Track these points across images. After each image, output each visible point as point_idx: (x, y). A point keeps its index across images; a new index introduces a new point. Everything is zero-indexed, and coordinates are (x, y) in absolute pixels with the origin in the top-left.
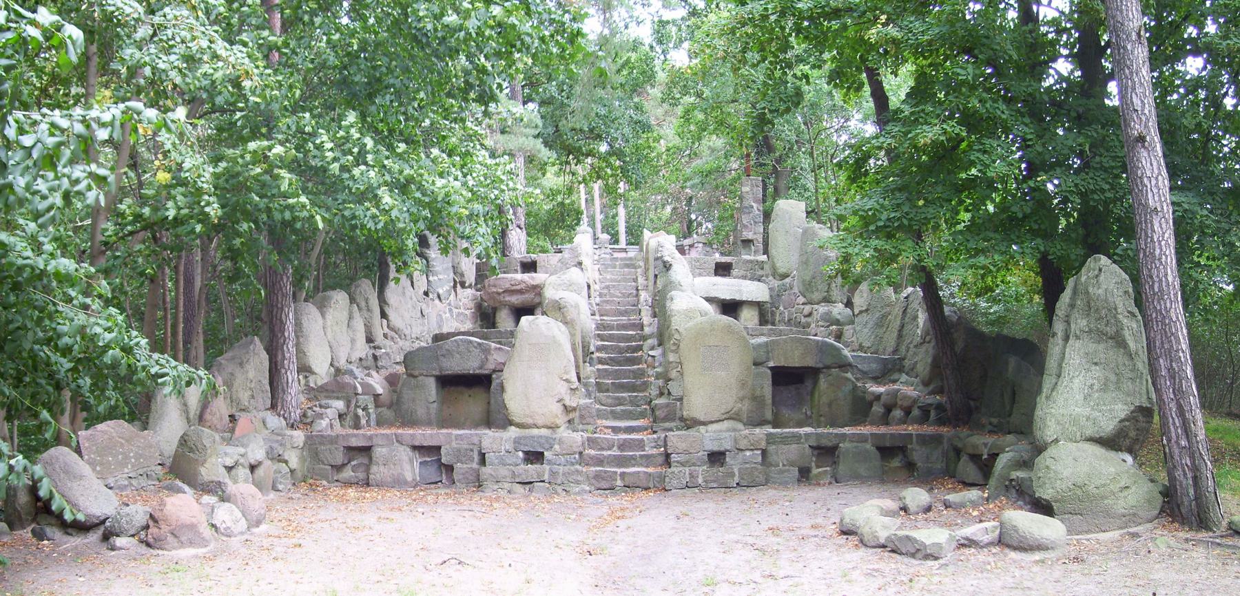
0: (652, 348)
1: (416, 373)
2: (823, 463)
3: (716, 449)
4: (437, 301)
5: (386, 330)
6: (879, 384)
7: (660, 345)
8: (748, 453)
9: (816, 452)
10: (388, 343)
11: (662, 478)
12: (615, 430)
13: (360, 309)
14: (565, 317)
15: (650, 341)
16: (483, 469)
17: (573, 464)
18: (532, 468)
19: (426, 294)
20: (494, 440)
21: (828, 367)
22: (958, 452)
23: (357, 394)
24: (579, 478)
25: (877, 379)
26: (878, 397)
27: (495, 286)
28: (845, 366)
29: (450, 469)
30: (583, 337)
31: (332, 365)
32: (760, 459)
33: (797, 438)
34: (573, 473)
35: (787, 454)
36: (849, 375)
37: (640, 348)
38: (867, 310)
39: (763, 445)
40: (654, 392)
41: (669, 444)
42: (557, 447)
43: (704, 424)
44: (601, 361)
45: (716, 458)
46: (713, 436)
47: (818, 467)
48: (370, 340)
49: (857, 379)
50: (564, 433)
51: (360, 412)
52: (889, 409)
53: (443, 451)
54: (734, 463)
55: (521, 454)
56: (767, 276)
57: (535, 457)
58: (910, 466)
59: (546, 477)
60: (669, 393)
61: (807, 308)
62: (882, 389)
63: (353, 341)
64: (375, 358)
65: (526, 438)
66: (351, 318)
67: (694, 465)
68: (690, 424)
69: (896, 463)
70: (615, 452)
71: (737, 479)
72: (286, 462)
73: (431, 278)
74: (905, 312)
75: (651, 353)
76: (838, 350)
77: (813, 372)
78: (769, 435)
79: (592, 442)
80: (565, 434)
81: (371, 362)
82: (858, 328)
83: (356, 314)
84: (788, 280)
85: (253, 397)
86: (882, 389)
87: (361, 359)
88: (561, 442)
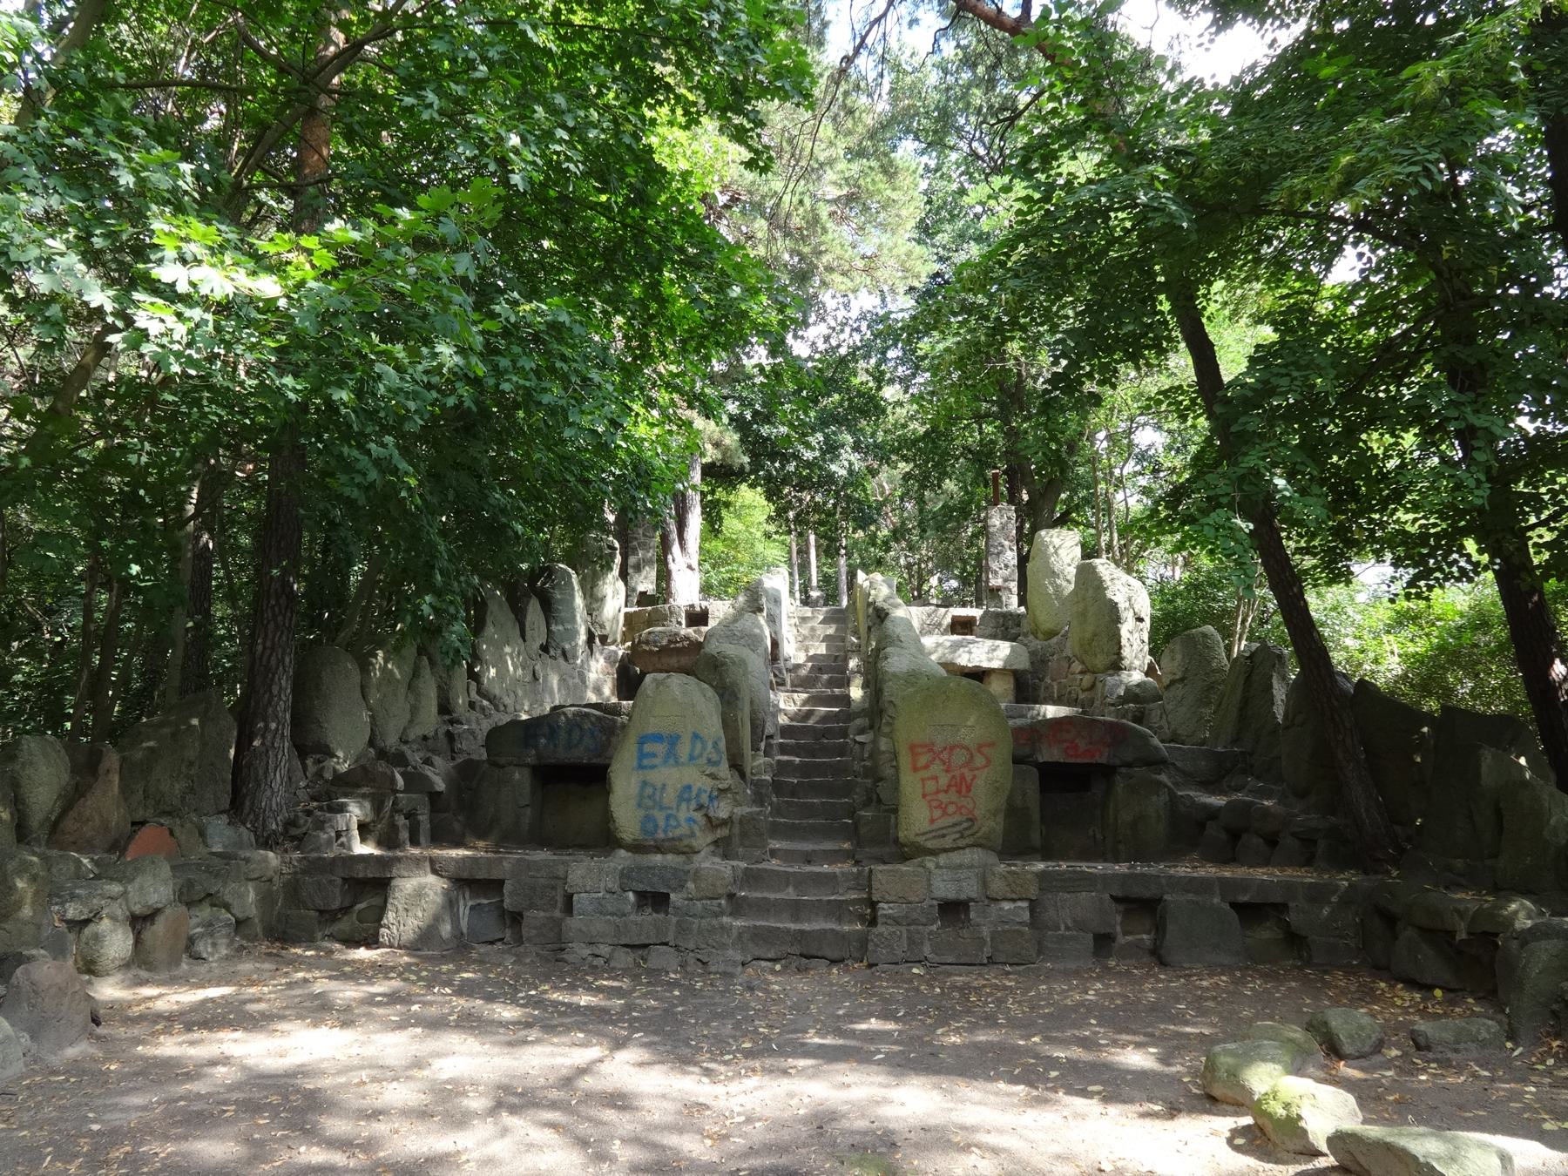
0: (861, 731)
1: (502, 761)
2: (1142, 931)
3: (952, 895)
4: (561, 660)
5: (474, 696)
6: (1213, 793)
7: (871, 727)
8: (1007, 906)
9: (1121, 908)
10: (474, 715)
11: (863, 941)
12: (788, 856)
13: (432, 663)
14: (722, 679)
15: (858, 721)
16: (569, 921)
17: (716, 915)
18: (649, 917)
19: (545, 649)
20: (590, 875)
21: (1129, 765)
22: (1391, 920)
23: (395, 791)
24: (725, 939)
25: (1209, 785)
26: (1212, 814)
27: (647, 643)
28: (1158, 763)
29: (516, 919)
30: (753, 712)
31: (371, 743)
32: (1026, 916)
33: (1089, 881)
34: (712, 930)
35: (1069, 909)
36: (1163, 778)
37: (844, 733)
38: (1182, 680)
39: (1033, 892)
40: (858, 798)
41: (875, 885)
42: (691, 885)
43: (934, 853)
44: (783, 749)
45: (953, 910)
46: (946, 878)
47: (1125, 933)
48: (445, 708)
49: (1176, 784)
50: (708, 863)
51: (401, 821)
52: (1235, 835)
53: (507, 888)
54: (984, 923)
55: (631, 895)
56: (1026, 635)
57: (655, 900)
58: (1294, 942)
59: (670, 938)
60: (879, 801)
61: (1087, 679)
62: (1218, 801)
63: (414, 710)
64: (450, 736)
65: (640, 868)
66: (416, 674)
67: (915, 922)
68: (905, 852)
69: (1266, 933)
70: (790, 894)
71: (987, 951)
72: (227, 907)
73: (554, 628)
74: (1248, 680)
75: (858, 738)
76: (1144, 737)
77: (1107, 771)
78: (1042, 876)
79: (751, 878)
80: (706, 865)
81: (443, 742)
82: (1169, 707)
83: (426, 672)
84: (1055, 640)
85: (192, 790)
86: (1218, 801)
87: (425, 738)
88: (697, 875)
